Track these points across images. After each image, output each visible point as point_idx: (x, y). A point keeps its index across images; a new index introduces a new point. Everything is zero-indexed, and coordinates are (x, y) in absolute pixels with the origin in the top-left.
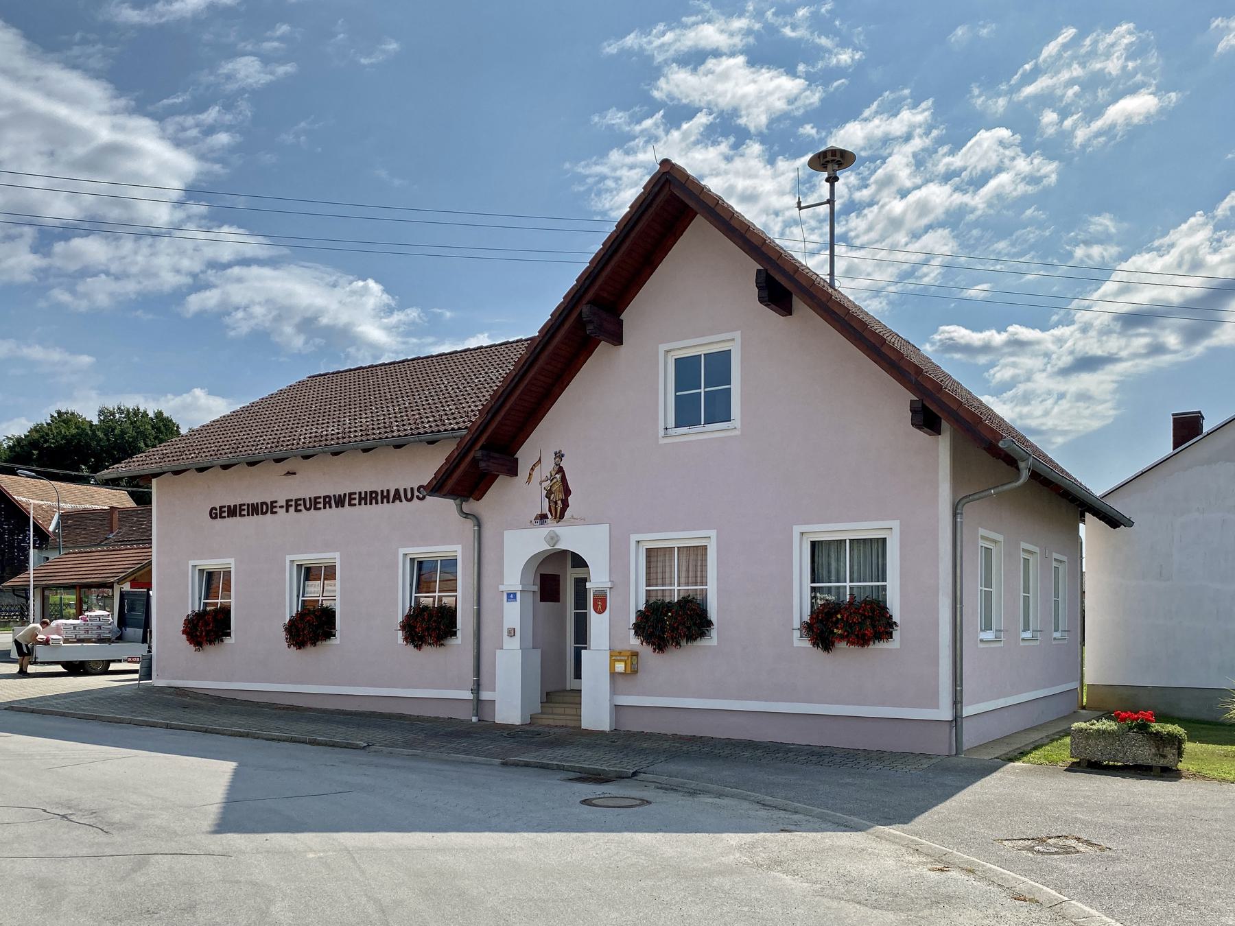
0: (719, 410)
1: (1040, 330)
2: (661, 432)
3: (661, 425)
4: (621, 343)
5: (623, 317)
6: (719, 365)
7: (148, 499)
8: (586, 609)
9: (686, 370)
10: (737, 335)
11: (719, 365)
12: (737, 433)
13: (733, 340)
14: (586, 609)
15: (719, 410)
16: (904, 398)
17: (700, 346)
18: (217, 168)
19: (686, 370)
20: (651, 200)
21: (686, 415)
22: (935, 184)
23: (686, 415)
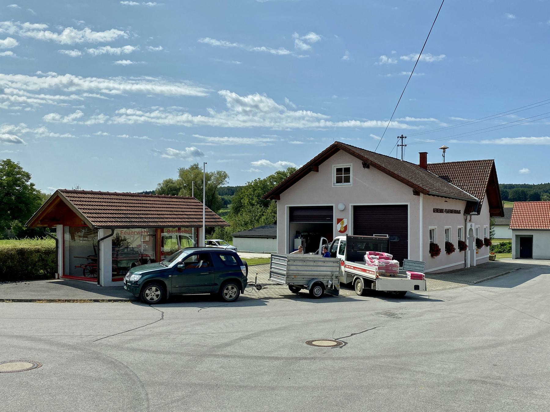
0: (347, 180)
1: (273, 99)
2: (333, 184)
3: (333, 183)
4: (318, 171)
5: (319, 166)
6: (347, 170)
7: (195, 231)
8: (336, 176)
9: (339, 170)
10: (352, 164)
11: (347, 170)
12: (352, 186)
13: (351, 165)
14: (336, 176)
15: (347, 180)
16: (411, 190)
17: (343, 166)
18: (166, 149)
19: (339, 170)
20: (71, 193)
21: (339, 181)
22: (48, 195)
23: (339, 181)
